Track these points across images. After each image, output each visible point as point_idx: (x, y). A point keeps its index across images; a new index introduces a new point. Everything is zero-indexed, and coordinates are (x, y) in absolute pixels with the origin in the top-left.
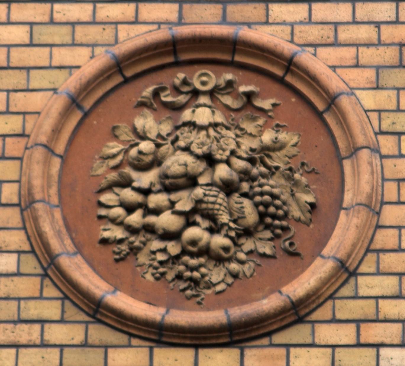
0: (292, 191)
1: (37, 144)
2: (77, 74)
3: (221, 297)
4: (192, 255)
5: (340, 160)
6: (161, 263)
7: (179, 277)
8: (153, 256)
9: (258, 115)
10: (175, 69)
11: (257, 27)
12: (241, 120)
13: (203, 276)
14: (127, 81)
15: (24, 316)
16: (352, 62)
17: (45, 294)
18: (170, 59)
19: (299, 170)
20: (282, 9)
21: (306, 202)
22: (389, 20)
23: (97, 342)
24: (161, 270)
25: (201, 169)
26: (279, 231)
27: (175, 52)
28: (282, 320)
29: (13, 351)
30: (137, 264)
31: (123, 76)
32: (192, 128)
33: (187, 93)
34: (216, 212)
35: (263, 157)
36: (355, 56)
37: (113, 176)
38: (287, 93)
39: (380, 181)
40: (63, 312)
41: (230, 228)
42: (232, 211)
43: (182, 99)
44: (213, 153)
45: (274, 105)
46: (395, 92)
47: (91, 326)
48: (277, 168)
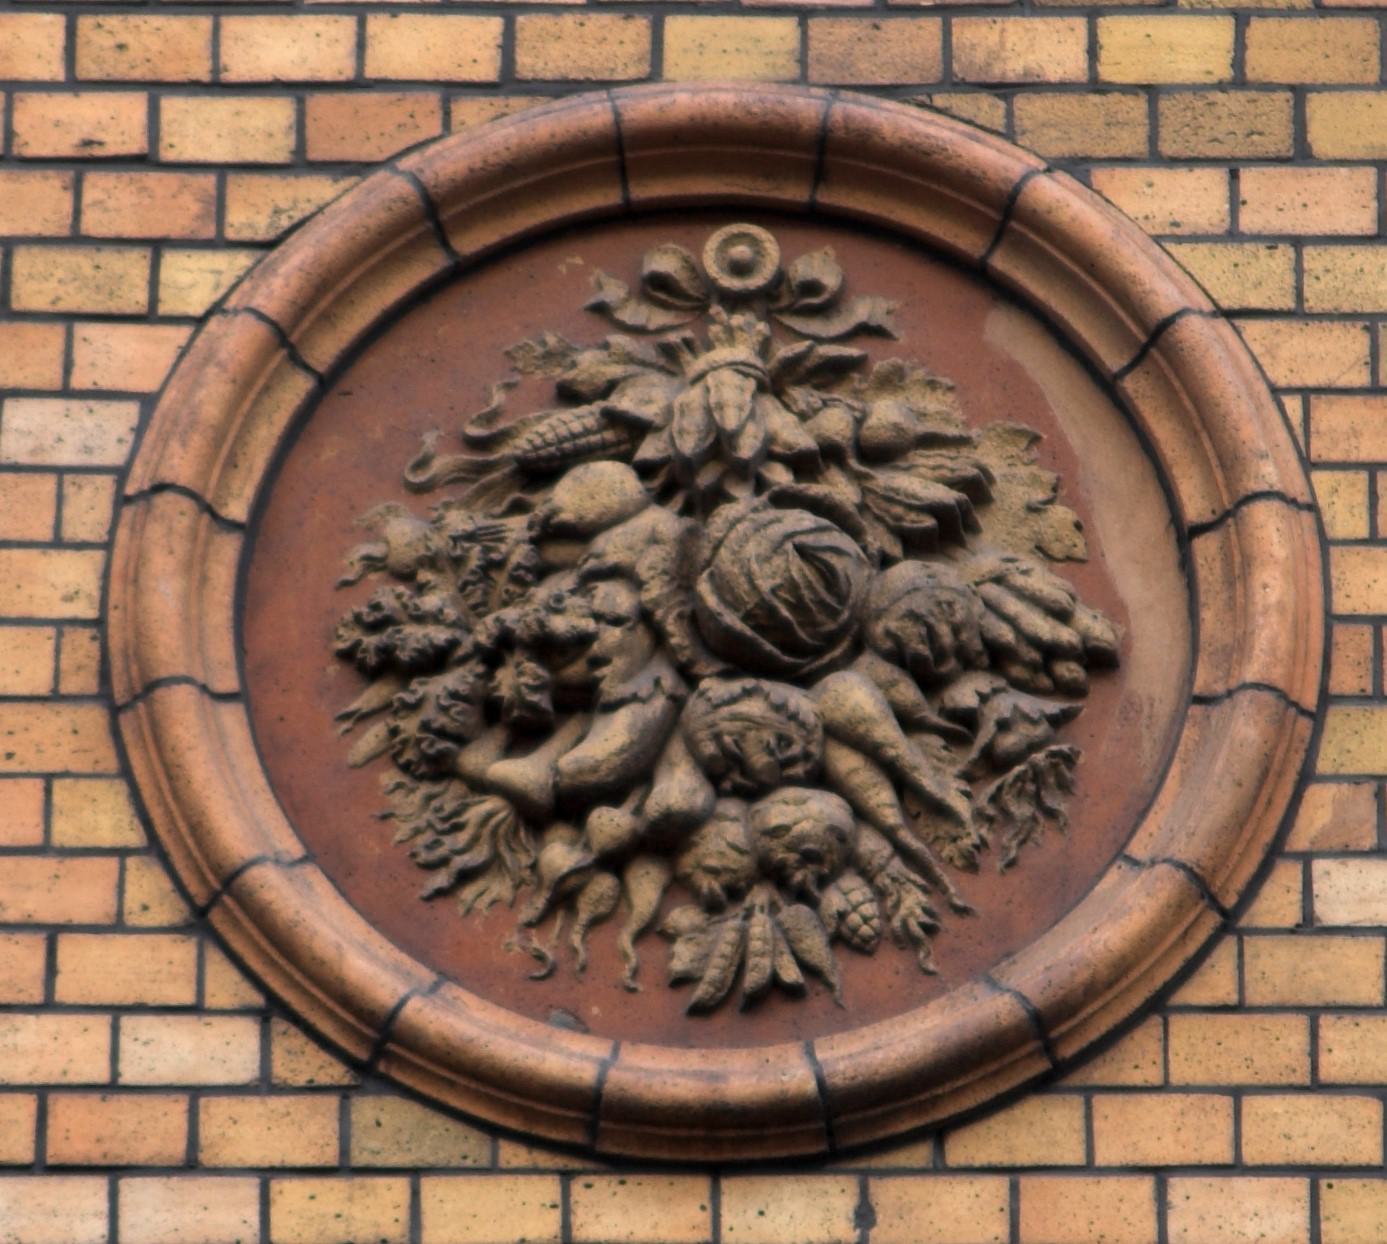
1: (160, 488)
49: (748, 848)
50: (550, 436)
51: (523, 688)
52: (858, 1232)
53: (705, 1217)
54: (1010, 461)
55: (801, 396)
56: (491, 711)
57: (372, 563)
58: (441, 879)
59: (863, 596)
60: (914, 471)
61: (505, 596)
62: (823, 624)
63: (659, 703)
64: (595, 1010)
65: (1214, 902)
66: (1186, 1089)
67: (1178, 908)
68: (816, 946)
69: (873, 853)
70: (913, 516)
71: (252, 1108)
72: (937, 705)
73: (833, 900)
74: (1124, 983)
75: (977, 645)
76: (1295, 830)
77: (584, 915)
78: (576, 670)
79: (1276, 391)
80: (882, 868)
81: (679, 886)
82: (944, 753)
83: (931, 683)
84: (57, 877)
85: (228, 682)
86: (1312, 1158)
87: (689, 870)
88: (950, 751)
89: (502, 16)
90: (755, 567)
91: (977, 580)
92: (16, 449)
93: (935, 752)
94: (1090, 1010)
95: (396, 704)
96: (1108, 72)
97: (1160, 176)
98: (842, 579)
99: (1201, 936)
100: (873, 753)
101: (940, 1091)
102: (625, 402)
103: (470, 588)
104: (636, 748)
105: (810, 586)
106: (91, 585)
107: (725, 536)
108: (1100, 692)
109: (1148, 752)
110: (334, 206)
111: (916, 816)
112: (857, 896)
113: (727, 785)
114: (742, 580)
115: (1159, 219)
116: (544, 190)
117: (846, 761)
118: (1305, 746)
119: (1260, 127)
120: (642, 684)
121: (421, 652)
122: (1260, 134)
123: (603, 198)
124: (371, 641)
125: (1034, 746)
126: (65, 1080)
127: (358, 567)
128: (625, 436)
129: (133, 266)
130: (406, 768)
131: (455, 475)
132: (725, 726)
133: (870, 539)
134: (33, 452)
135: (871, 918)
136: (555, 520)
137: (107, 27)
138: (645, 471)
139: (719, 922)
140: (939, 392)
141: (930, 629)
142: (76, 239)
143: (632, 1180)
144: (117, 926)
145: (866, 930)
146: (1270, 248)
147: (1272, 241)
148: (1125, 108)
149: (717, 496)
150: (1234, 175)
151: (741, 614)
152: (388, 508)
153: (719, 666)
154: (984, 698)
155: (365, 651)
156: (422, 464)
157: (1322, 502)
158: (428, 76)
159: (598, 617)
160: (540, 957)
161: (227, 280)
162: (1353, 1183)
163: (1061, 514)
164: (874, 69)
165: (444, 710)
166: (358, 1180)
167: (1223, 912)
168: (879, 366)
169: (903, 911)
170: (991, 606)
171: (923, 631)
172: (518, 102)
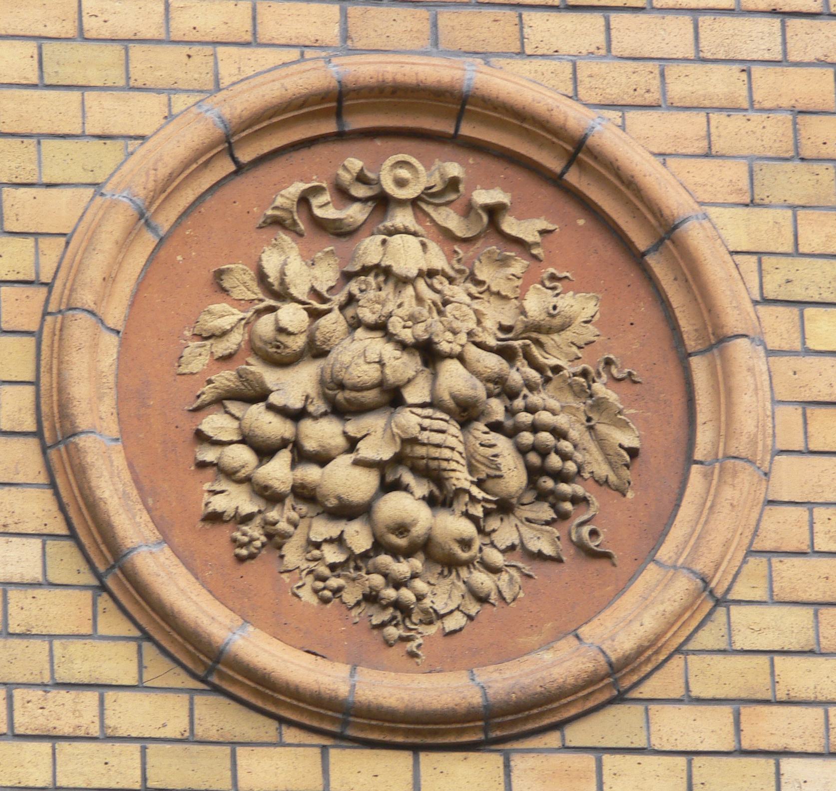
0: (589, 419)
3: (455, 640)
4: (397, 553)
5: (683, 358)
6: (333, 567)
7: (371, 598)
8: (316, 553)
9: (513, 254)
10: (338, 148)
11: (502, 62)
12: (477, 263)
13: (420, 598)
14: (241, 169)
15: (63, 675)
16: (700, 146)
17: (102, 630)
18: (329, 127)
19: (599, 375)
20: (549, 24)
21: (621, 446)
22: (767, 57)
23: (214, 735)
24: (334, 582)
25: (411, 373)
26: (568, 506)
27: (338, 113)
28: (586, 698)
29: (45, 747)
30: (282, 569)
31: (235, 160)
32: (381, 278)
33: (364, 200)
34: (444, 464)
35: (529, 345)
36: (703, 133)
37: (226, 378)
38: (569, 209)
39: (769, 405)
40: (141, 667)
41: (473, 499)
42: (473, 461)
43: (355, 213)
44: (436, 340)
45: (543, 232)
46: (789, 213)
47: (199, 699)
48: (557, 369)
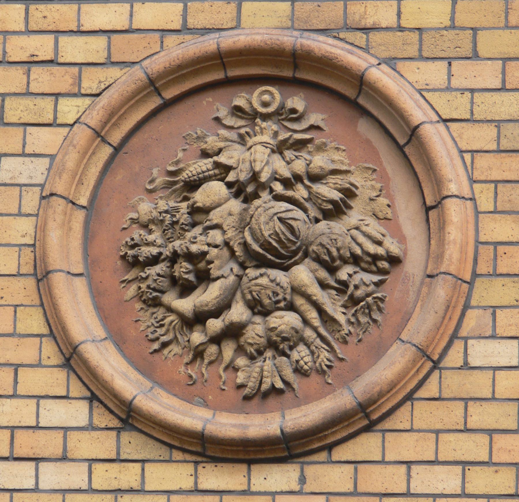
1: (52, 195)
2: (104, 101)
49: (263, 335)
50: (194, 172)
51: (182, 274)
52: (299, 486)
53: (245, 480)
54: (365, 179)
55: (289, 154)
56: (174, 281)
57: (133, 221)
58: (156, 346)
59: (306, 236)
60: (328, 185)
61: (179, 235)
62: (290, 247)
63: (232, 278)
64: (210, 397)
65: (429, 358)
66: (419, 431)
67: (414, 362)
68: (289, 374)
69: (309, 337)
70: (325, 204)
71: (85, 435)
72: (334, 278)
73: (295, 355)
74: (394, 390)
75: (348, 254)
76: (462, 328)
77: (206, 361)
78: (202, 265)
79: (461, 152)
80: (312, 343)
81: (240, 350)
82: (336, 297)
83: (332, 270)
84: (18, 345)
85: (79, 269)
86: (463, 459)
87: (243, 344)
88: (339, 296)
89: (183, 3)
90: (262, 227)
91: (349, 228)
92: (6, 178)
93: (333, 297)
94: (381, 401)
95: (139, 278)
96: (404, 23)
97: (422, 64)
98: (297, 230)
99: (424, 371)
100: (308, 298)
101: (326, 433)
102: (222, 159)
103: (166, 232)
104: (222, 296)
105: (283, 233)
106: (31, 231)
107: (254, 213)
108: (396, 272)
109: (412, 296)
110: (119, 80)
111: (326, 322)
112: (303, 354)
113: (256, 310)
114: (259, 231)
115: (421, 83)
116: (196, 73)
117: (299, 301)
118: (466, 295)
119: (459, 45)
120: (226, 271)
121: (147, 258)
122: (460, 47)
123: (218, 75)
124: (130, 252)
125: (368, 295)
126: (20, 425)
127: (129, 222)
128: (223, 171)
129: (48, 103)
130: (144, 302)
131: (164, 185)
132: (253, 288)
133: (310, 213)
134: (11, 178)
135: (308, 363)
136: (195, 206)
137: (40, 10)
138: (229, 185)
139: (255, 363)
140: (340, 152)
141: (328, 250)
142: (28, 94)
143: (219, 465)
144: (39, 365)
145: (306, 367)
146: (462, 94)
147: (463, 91)
148: (410, 38)
149: (256, 196)
150: (450, 64)
151: (259, 244)
152: (140, 199)
153: (254, 263)
154: (350, 276)
155: (128, 256)
156: (152, 181)
157: (477, 197)
158: (155, 28)
159: (209, 245)
160: (191, 377)
161: (82, 110)
162: (477, 468)
163: (383, 201)
164: (318, 23)
165: (155, 280)
166: (123, 464)
167: (433, 361)
168: (317, 142)
169: (320, 360)
170: (354, 239)
171: (325, 251)
172: (188, 37)
